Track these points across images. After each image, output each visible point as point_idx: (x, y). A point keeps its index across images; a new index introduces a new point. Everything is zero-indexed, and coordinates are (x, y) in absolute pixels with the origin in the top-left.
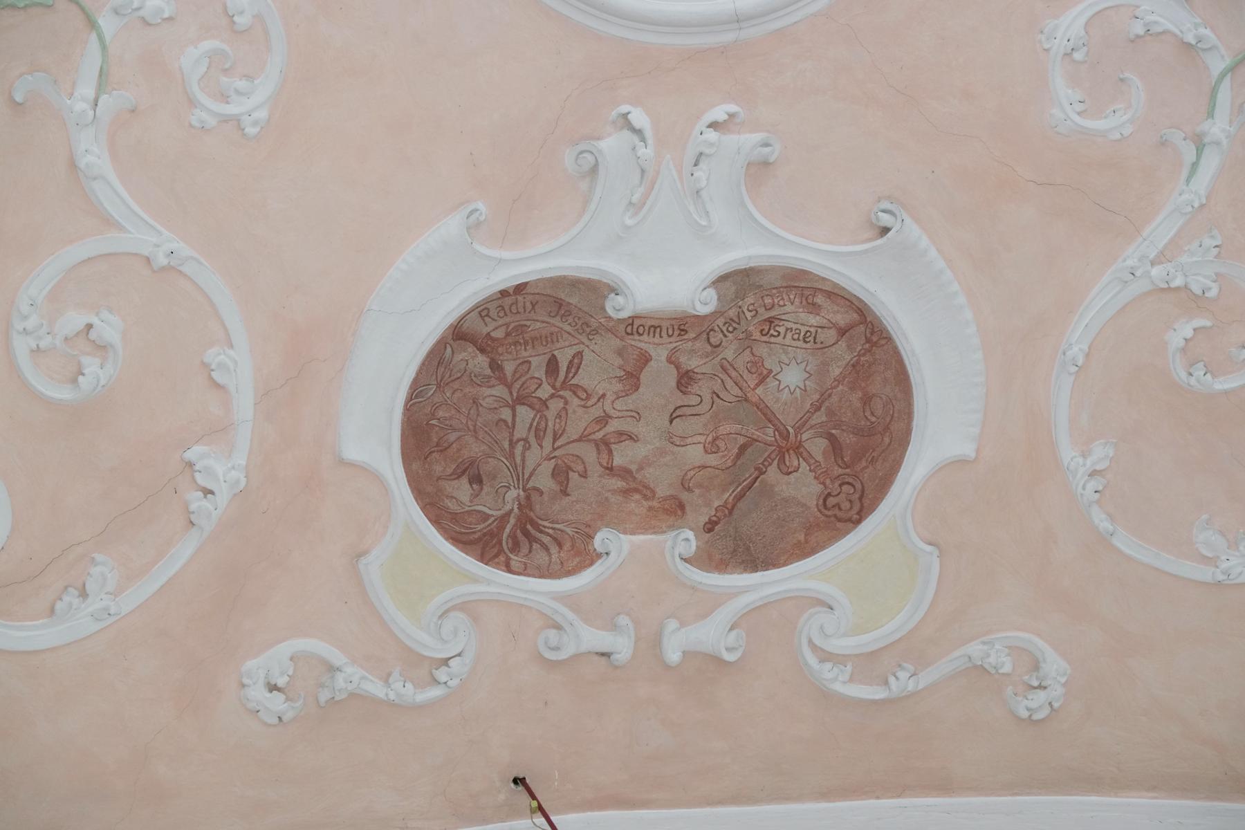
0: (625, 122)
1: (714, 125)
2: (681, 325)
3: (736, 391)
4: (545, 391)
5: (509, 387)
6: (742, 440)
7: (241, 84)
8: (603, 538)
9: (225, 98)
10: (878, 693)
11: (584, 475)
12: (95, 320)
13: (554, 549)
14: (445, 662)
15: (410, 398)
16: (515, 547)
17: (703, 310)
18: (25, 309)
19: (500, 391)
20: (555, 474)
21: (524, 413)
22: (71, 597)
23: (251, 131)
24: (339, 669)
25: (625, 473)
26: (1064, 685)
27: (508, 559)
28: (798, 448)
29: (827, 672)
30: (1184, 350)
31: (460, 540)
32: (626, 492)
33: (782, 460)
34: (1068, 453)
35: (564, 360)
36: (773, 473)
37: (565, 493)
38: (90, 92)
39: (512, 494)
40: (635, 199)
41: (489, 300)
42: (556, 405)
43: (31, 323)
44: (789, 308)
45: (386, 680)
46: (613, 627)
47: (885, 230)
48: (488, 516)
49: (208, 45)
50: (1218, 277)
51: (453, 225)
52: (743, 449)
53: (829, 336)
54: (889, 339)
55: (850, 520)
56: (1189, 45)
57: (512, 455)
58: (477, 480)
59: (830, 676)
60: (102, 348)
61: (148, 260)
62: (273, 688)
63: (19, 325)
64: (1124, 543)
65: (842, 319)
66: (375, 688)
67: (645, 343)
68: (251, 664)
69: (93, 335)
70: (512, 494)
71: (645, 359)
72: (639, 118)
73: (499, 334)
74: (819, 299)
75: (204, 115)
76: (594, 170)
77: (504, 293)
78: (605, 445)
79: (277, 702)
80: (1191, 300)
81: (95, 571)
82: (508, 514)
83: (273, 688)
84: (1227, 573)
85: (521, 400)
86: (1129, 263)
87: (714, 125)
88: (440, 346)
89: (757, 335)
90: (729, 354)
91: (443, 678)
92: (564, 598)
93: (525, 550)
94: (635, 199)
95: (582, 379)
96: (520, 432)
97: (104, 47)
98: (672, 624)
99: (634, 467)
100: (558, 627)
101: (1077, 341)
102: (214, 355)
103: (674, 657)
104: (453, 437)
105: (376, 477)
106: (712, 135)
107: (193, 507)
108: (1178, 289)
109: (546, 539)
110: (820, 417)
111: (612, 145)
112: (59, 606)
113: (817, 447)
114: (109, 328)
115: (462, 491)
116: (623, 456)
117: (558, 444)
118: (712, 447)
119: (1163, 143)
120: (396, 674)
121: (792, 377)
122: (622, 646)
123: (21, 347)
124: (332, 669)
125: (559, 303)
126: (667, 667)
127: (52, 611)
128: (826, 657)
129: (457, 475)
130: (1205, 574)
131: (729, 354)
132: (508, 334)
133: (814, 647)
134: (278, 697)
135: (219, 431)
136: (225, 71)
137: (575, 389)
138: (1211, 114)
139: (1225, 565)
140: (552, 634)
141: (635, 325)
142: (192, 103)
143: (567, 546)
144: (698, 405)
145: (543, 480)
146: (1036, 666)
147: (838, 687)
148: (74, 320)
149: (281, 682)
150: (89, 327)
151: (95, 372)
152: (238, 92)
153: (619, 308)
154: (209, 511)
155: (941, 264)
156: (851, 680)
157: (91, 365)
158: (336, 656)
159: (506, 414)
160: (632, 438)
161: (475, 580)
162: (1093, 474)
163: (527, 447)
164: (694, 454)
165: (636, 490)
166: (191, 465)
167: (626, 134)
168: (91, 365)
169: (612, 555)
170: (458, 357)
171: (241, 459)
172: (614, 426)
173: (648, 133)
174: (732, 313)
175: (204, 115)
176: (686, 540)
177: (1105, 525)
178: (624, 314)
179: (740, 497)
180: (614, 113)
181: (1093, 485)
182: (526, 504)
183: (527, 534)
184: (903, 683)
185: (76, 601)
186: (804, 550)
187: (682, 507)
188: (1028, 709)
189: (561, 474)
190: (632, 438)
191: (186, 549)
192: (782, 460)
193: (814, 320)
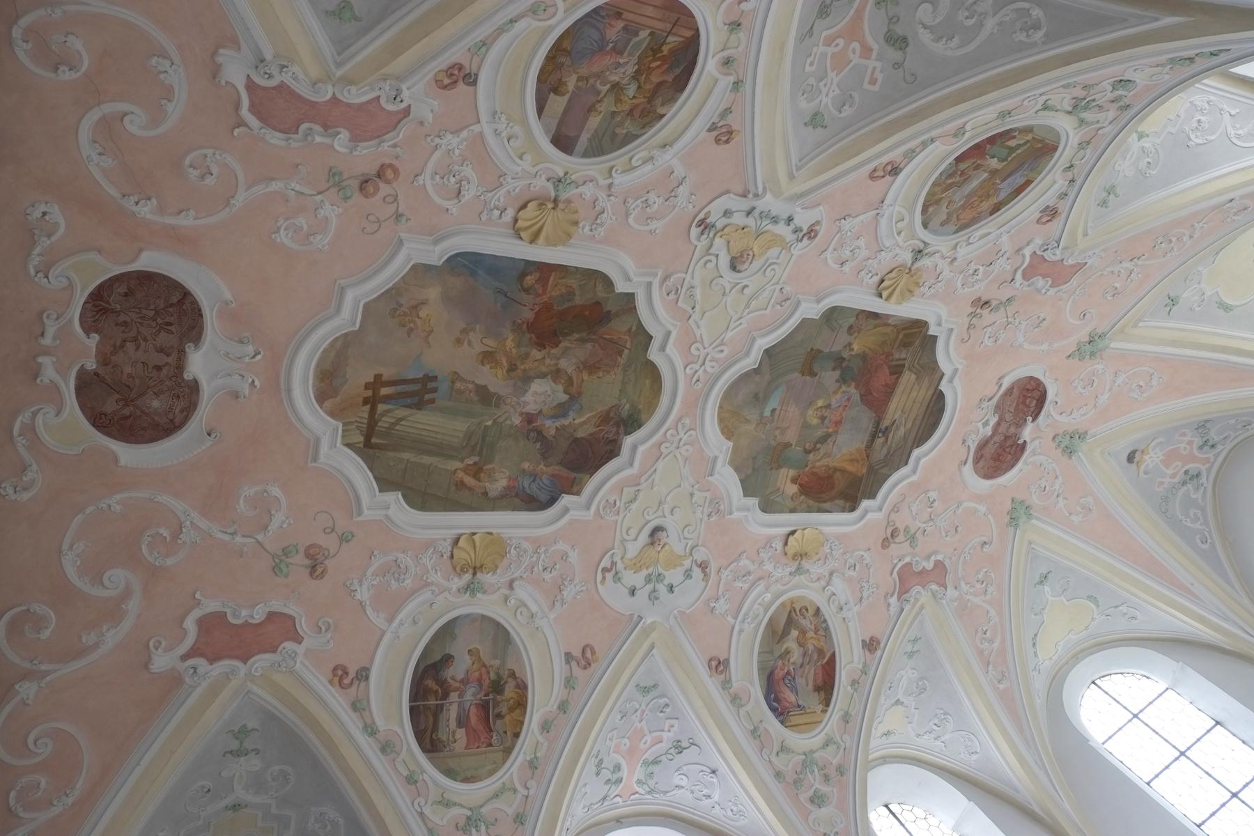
0: (257, 353)
1: (253, 381)
2: (180, 367)
3: (152, 384)
4: (159, 321)
5: (163, 309)
6: (132, 386)
7: (290, 235)
8: (95, 337)
9: (286, 229)
10: (16, 432)
11: (123, 332)
12: (213, 177)
13: (92, 319)
14: (47, 277)
15: (163, 275)
16: (95, 306)
17: (185, 376)
18: (224, 156)
19: (162, 306)
20: (125, 322)
21: (151, 313)
22: (100, 150)
23: (273, 236)
24: (49, 238)
25: (122, 346)
26: (16, 500)
27: (89, 303)
28: (127, 405)
29: (28, 414)
30: (158, 533)
31: (100, 288)
32: (114, 346)
33: (121, 400)
34: (118, 497)
35: (172, 328)
36: (117, 396)
37: (117, 325)
38: (297, 189)
39: (118, 307)
40: (230, 355)
41: (198, 305)
42: (154, 324)
43: (218, 157)
44: (183, 403)
45: (39, 255)
46: (55, 338)
47: (209, 435)
48: (110, 297)
49: (305, 227)
50: (185, 543)
51: (228, 296)
52: (128, 387)
53: (171, 416)
54: (167, 436)
55: (94, 423)
56: (267, 527)
57: (134, 307)
58: (126, 295)
59: (26, 416)
60: (203, 177)
61: (233, 197)
62: (44, 214)
63: (217, 152)
64: (80, 517)
65: (177, 421)
66: (37, 250)
67: (175, 355)
68: (56, 207)
69: (208, 175)
70: (118, 307)
71: (168, 355)
72: (259, 357)
73: (184, 307)
74: (185, 413)
75: (282, 222)
76: (242, 342)
77: (200, 310)
78: (135, 339)
79: (37, 214)
80: (176, 535)
81: (110, 160)
82: (109, 304)
83: (44, 214)
84: (66, 554)
85: (157, 313)
86: (192, 515)
87: (253, 381)
88: (183, 287)
89: (173, 392)
90: (167, 383)
91: (39, 275)
92: (71, 321)
93: (93, 309)
94: (230, 355)
95: (163, 334)
96: (144, 311)
97: (311, 195)
98: (54, 359)
99: (125, 349)
100: (57, 319)
101: (164, 498)
102: (192, 213)
103: (40, 360)
104: (146, 288)
105: (132, 261)
106: (250, 380)
107: (131, 198)
108: (181, 530)
109: (97, 317)
110: (138, 413)
111: (250, 349)
112: (98, 145)
113: (126, 412)
114: (209, 181)
115: (122, 289)
116: (130, 346)
117: (138, 324)
118: (130, 376)
119: (234, 522)
120: (42, 258)
121: (156, 404)
122: (47, 341)
123: (209, 152)
124: (49, 236)
125: (194, 328)
126: (35, 357)
127: (95, 142)
128: (35, 414)
129: (129, 288)
130: (65, 546)
131: (167, 383)
132: (183, 310)
133: (39, 410)
134: (39, 215)
135: (161, 210)
136: (295, 231)
137: (159, 331)
138: (243, 536)
139: (69, 553)
140: (55, 316)
141: (182, 354)
142: (286, 219)
143: (94, 324)
144: (322, 511)
145: (122, 318)
146: (25, 489)
147: (20, 418)
148: (215, 170)
149: (47, 218)
150: (212, 175)
151: (194, 174)
152: (287, 234)
153: (189, 348)
154: (129, 203)
155: (195, 453)
156: (22, 422)
157: (197, 173)
158: (54, 239)
159: (152, 307)
160: (137, 349)
161: (83, 290)
162: (110, 506)
163: (137, 313)
164: (128, 370)
165: (115, 349)
166: (149, 199)
167: (253, 354)
168: (197, 173)
169: (88, 340)
170: (177, 293)
171: (148, 216)
172: (143, 343)
173: (253, 360)
174: (183, 384)
175: (282, 222)
176: (91, 365)
177: (88, 511)
178: (187, 349)
179: (108, 385)
180: (260, 349)
181: (105, 506)
182: (113, 311)
183: (100, 310)
184: (20, 442)
185: (98, 151)
186: (83, 407)
187: (106, 365)
188: (5, 487)
189: (125, 324)
190: (137, 349)
191: (114, 192)
192: (121, 400)
193: (177, 411)
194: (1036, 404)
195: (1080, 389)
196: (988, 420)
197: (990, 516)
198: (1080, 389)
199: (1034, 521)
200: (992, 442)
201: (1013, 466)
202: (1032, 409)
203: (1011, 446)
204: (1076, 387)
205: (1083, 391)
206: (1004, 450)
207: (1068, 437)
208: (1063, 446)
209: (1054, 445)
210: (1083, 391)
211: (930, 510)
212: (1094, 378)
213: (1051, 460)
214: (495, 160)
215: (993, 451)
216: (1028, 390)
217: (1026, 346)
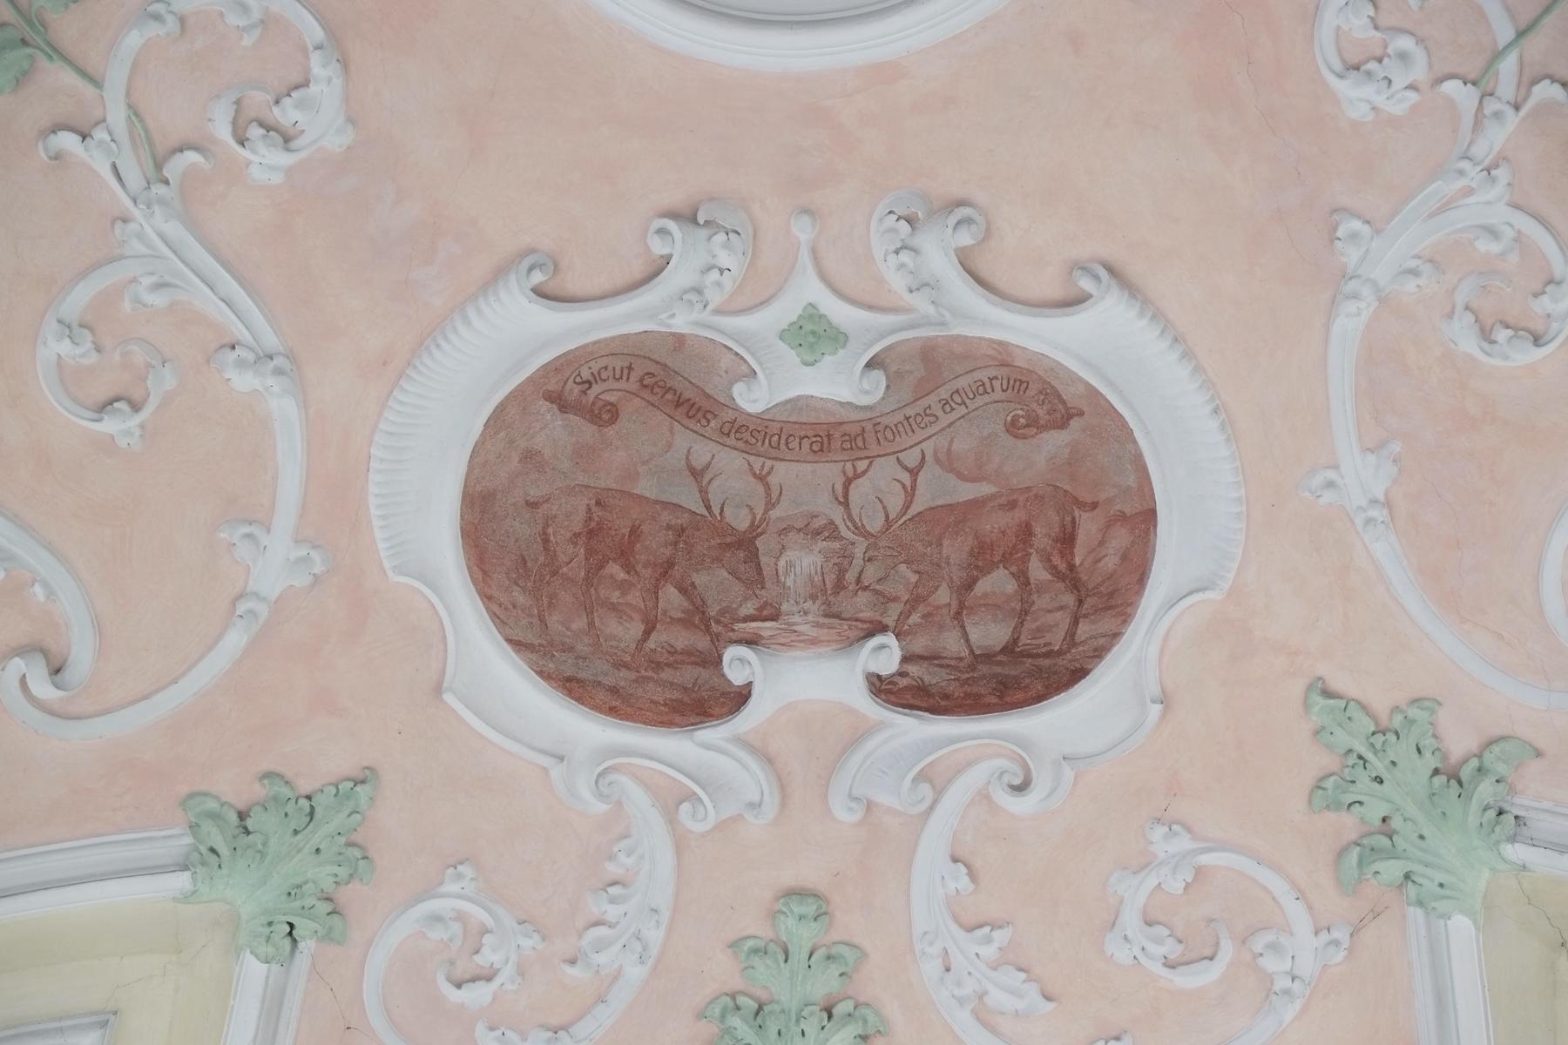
194: (987, 657)
195: (1135, 893)
196: (835, 337)
197: (236, 640)
198: (1135, 893)
199: (254, 972)
200: (703, 451)
201: (574, 687)
202: (951, 643)
203: (698, 616)
204: (1145, 864)
205: (1131, 920)
206: (665, 570)
207: (824, 984)
208: (770, 979)
209: (754, 926)
210: (1131, 920)
211: (223, 132)
212: (1227, 951)
213: (655, 936)
214: (1554, 526)
215: (646, 487)
216: (1067, 540)
217: (1351, 322)
